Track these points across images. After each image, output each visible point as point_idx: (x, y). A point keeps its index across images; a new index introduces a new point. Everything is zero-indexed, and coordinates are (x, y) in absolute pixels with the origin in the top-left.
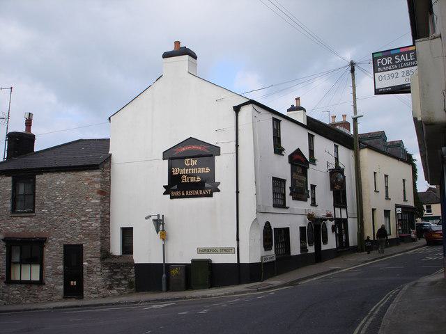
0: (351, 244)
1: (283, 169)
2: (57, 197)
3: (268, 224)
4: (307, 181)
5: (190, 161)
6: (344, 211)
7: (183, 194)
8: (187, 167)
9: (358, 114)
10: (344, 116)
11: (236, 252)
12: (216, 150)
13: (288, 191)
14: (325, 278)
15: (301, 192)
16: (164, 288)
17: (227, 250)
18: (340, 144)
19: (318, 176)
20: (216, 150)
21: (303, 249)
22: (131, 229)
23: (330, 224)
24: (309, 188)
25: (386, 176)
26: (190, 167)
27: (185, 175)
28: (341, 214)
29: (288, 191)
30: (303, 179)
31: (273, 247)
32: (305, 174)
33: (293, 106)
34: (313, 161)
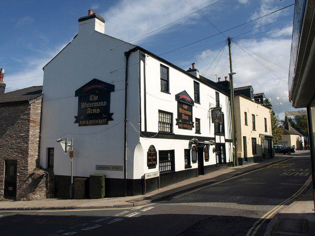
0: (227, 161)
1: (172, 106)
2: (3, 124)
3: (152, 147)
4: (192, 115)
5: (93, 97)
6: (222, 138)
7: (88, 123)
8: (91, 102)
9: (233, 72)
10: (226, 78)
11: (124, 171)
12: (110, 88)
13: (175, 122)
14: (199, 191)
15: (186, 120)
16: (104, 194)
17: (117, 168)
18: (221, 92)
19: (201, 112)
20: (110, 88)
21: (188, 165)
22: (53, 149)
23: (212, 147)
24: (194, 120)
25: (253, 115)
26: (93, 102)
27: (89, 108)
28: (220, 139)
29: (175, 122)
30: (188, 113)
31: (157, 166)
32: (190, 110)
33: (190, 68)
34: (198, 100)
